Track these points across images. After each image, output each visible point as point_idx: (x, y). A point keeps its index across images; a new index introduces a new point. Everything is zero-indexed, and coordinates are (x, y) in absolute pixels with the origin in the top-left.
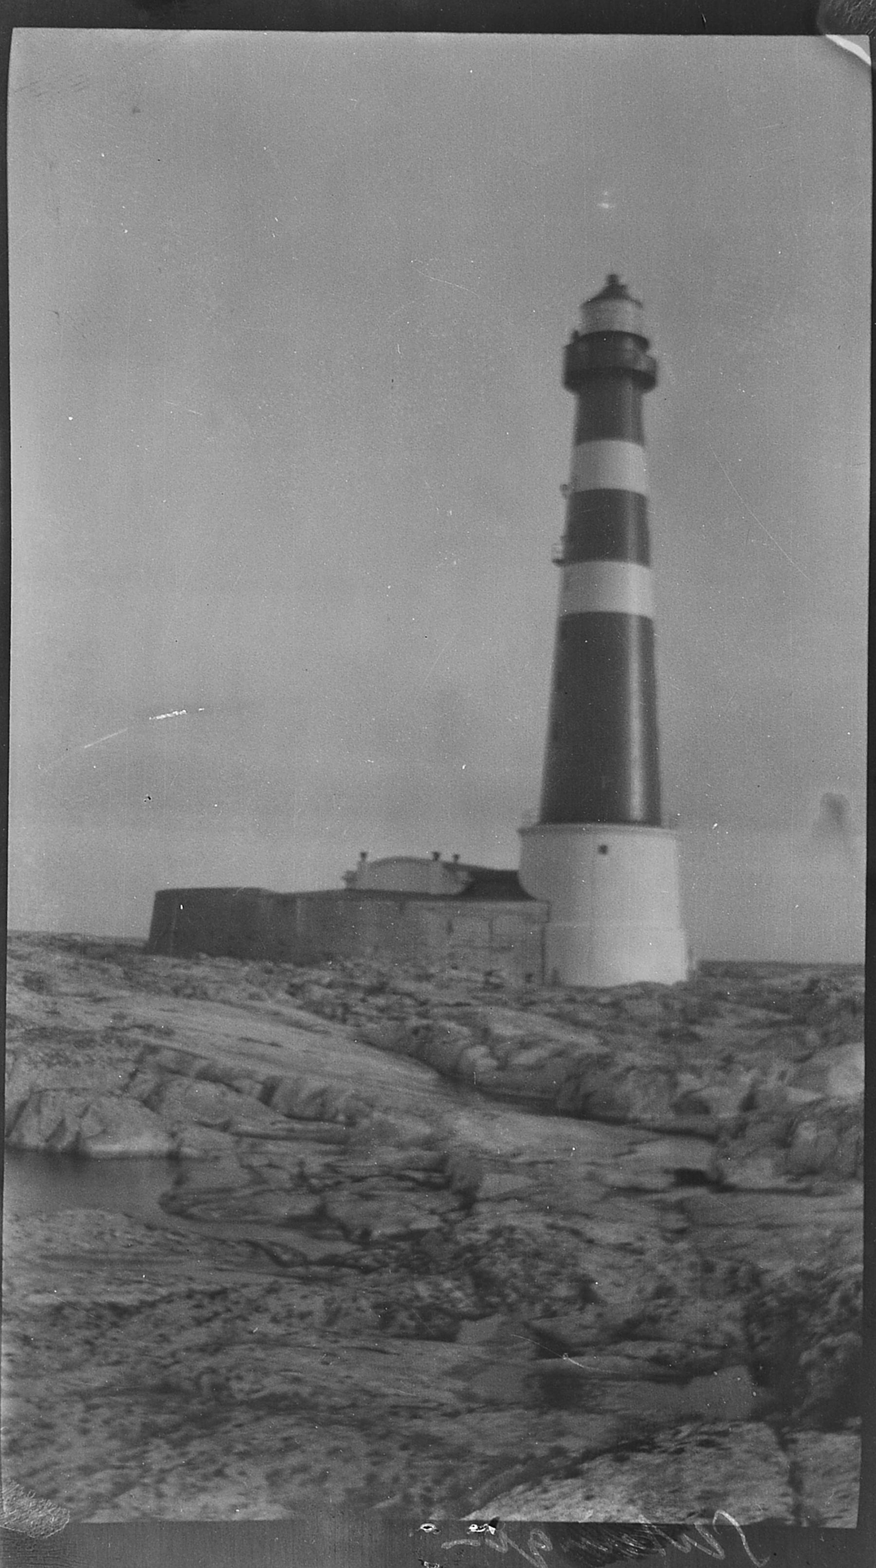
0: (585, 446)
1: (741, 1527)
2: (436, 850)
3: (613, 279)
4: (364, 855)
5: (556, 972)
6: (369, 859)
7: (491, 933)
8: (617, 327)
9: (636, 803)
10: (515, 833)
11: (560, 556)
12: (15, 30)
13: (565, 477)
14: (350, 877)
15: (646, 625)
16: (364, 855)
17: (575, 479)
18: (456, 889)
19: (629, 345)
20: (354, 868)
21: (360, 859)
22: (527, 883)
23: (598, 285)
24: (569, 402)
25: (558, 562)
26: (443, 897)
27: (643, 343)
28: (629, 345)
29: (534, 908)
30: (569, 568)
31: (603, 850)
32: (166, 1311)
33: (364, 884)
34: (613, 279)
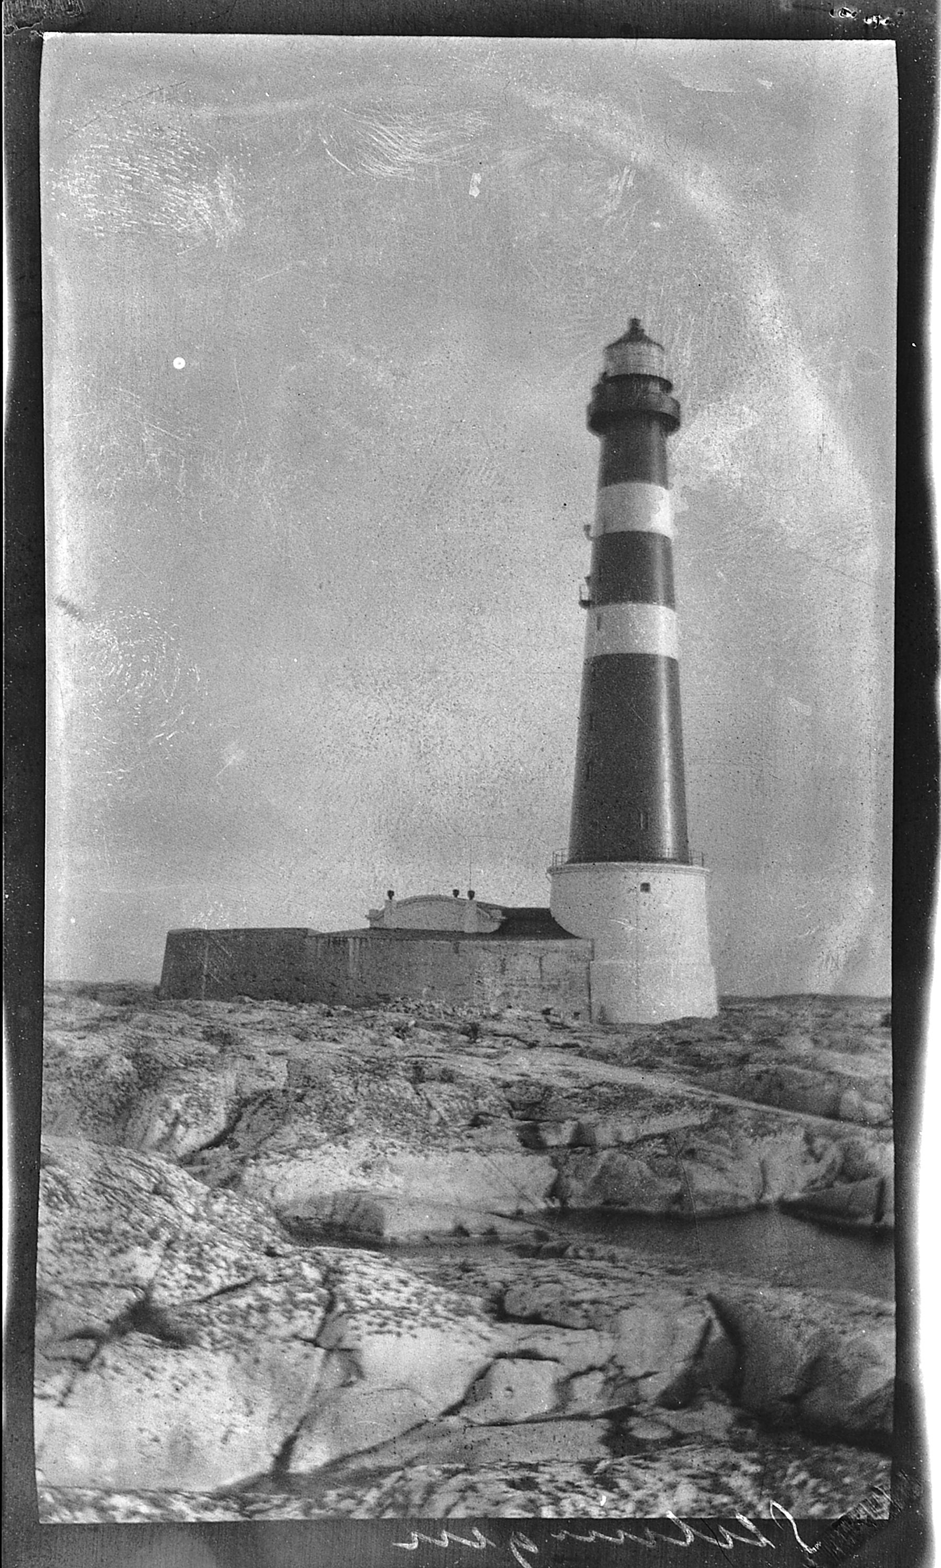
0: (614, 488)
1: (795, 1520)
2: (456, 888)
3: (635, 323)
4: (391, 894)
5: (602, 1010)
6: (396, 898)
7: (542, 971)
8: (645, 371)
9: (668, 842)
10: (652, 890)
11: (586, 597)
12: (892, 43)
13: (590, 517)
14: (374, 916)
15: (672, 664)
16: (391, 894)
17: (604, 518)
18: (495, 926)
19: (655, 388)
20: (380, 906)
21: (387, 898)
22: (564, 920)
23: (622, 329)
24: (593, 444)
25: (585, 604)
26: (479, 935)
27: (667, 386)
28: (655, 388)
29: (578, 946)
30: (600, 609)
31: (646, 887)
32: (606, 1482)
33: (392, 922)
34: (635, 323)
